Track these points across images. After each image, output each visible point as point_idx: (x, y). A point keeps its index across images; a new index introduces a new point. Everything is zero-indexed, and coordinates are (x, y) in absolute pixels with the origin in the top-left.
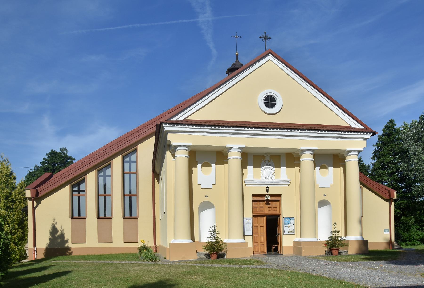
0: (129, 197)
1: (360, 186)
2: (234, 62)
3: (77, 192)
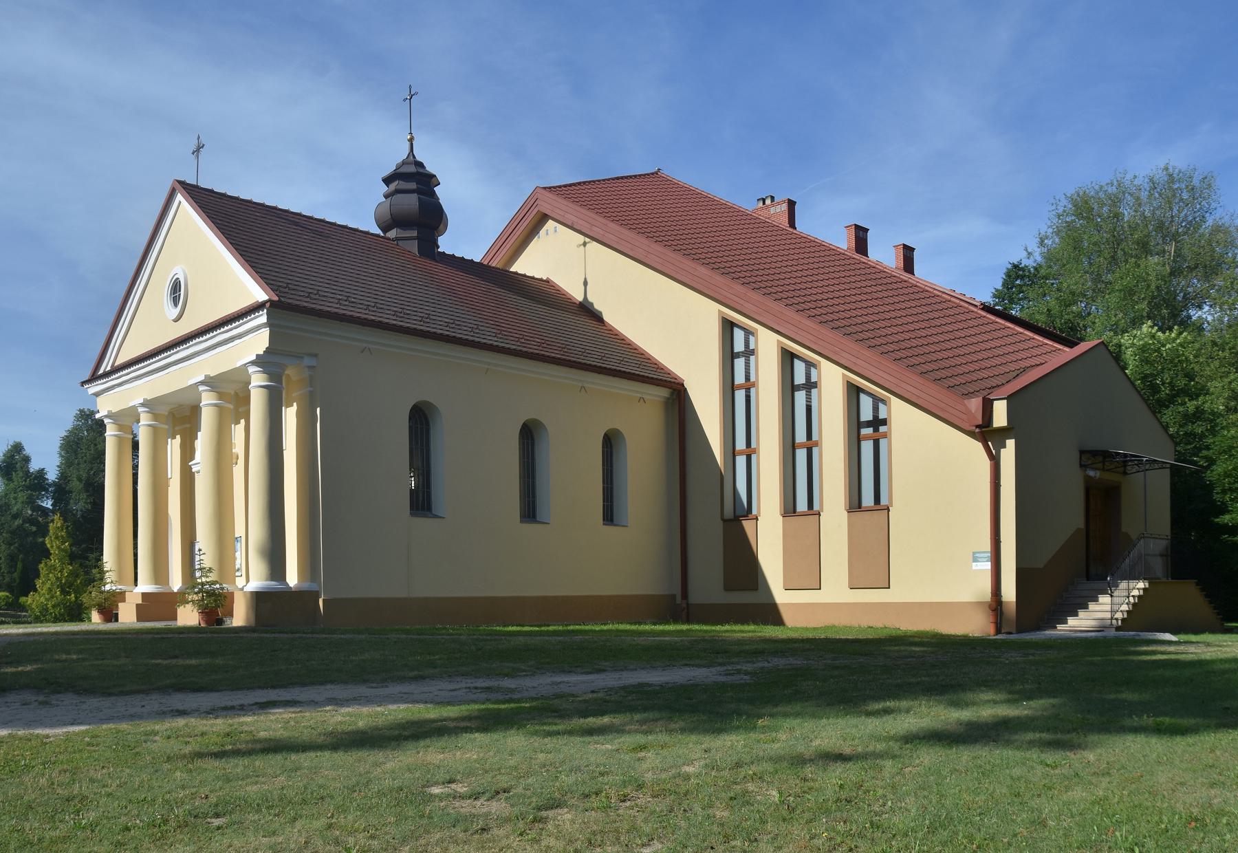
0: (806, 449)
1: (843, 374)
2: (403, 155)
3: (872, 429)
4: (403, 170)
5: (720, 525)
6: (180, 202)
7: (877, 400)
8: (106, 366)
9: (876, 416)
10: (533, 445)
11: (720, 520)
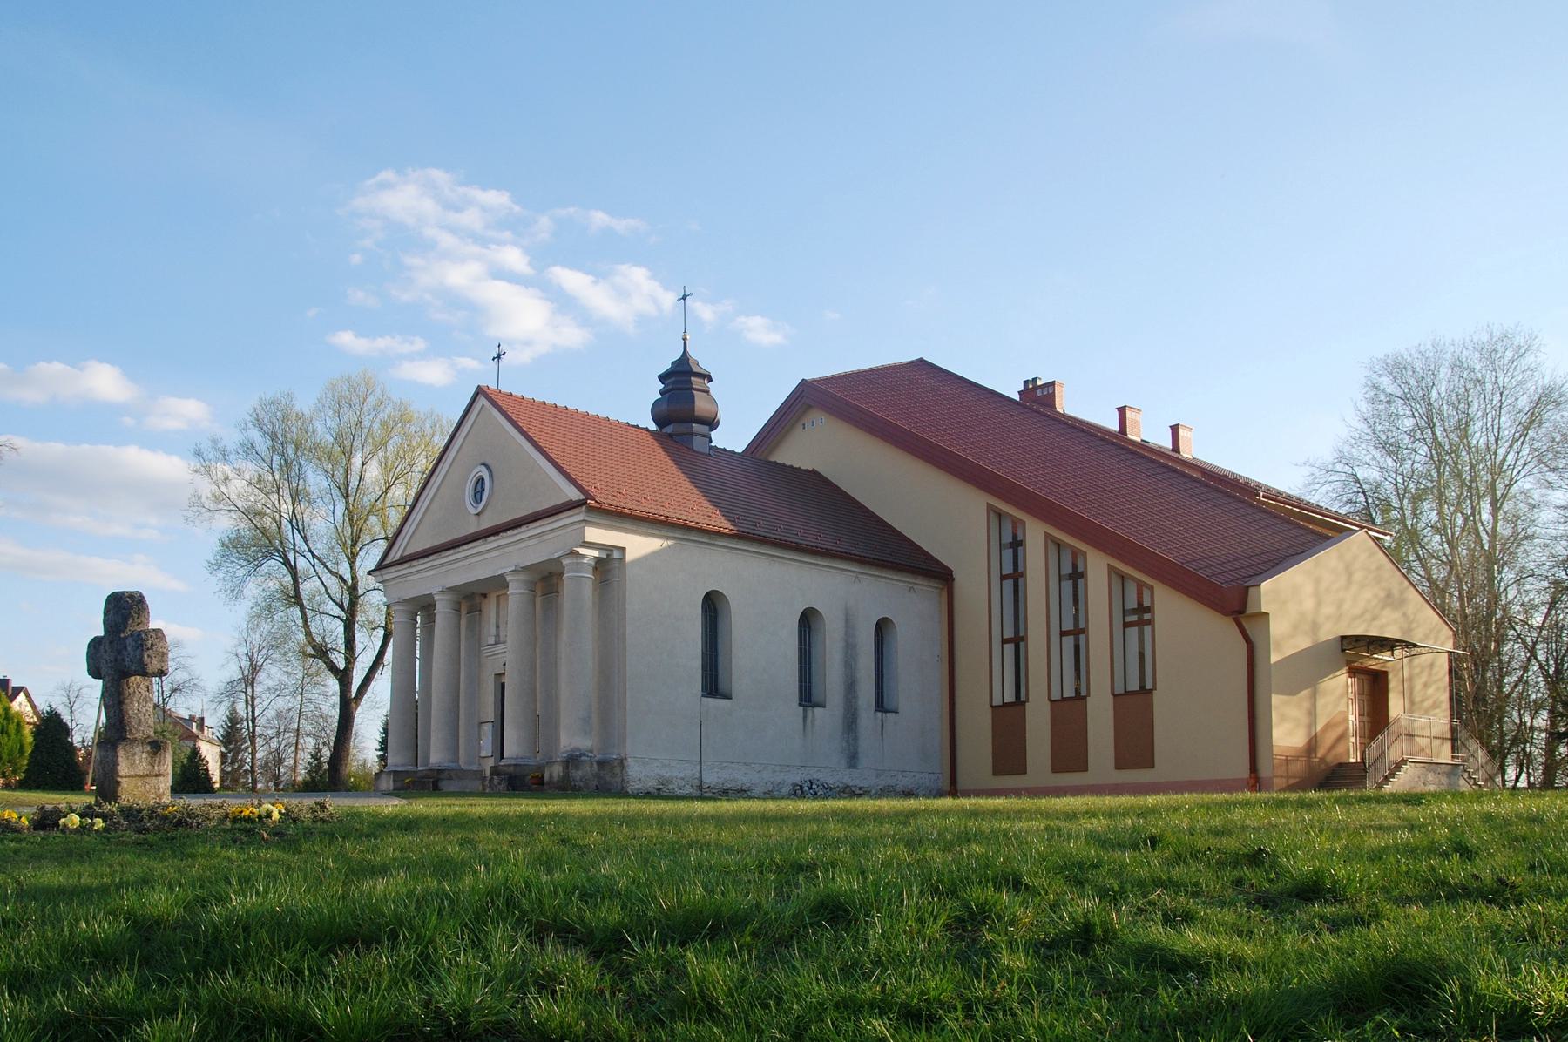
4: (678, 369)
5: (1047, 705)
6: (483, 405)
7: (1141, 586)
8: (388, 560)
9: (1140, 604)
10: (716, 618)
11: (988, 706)
